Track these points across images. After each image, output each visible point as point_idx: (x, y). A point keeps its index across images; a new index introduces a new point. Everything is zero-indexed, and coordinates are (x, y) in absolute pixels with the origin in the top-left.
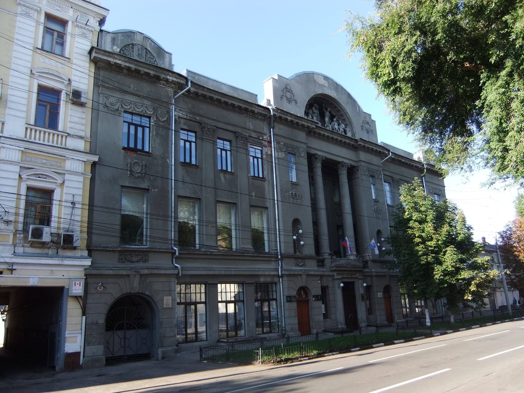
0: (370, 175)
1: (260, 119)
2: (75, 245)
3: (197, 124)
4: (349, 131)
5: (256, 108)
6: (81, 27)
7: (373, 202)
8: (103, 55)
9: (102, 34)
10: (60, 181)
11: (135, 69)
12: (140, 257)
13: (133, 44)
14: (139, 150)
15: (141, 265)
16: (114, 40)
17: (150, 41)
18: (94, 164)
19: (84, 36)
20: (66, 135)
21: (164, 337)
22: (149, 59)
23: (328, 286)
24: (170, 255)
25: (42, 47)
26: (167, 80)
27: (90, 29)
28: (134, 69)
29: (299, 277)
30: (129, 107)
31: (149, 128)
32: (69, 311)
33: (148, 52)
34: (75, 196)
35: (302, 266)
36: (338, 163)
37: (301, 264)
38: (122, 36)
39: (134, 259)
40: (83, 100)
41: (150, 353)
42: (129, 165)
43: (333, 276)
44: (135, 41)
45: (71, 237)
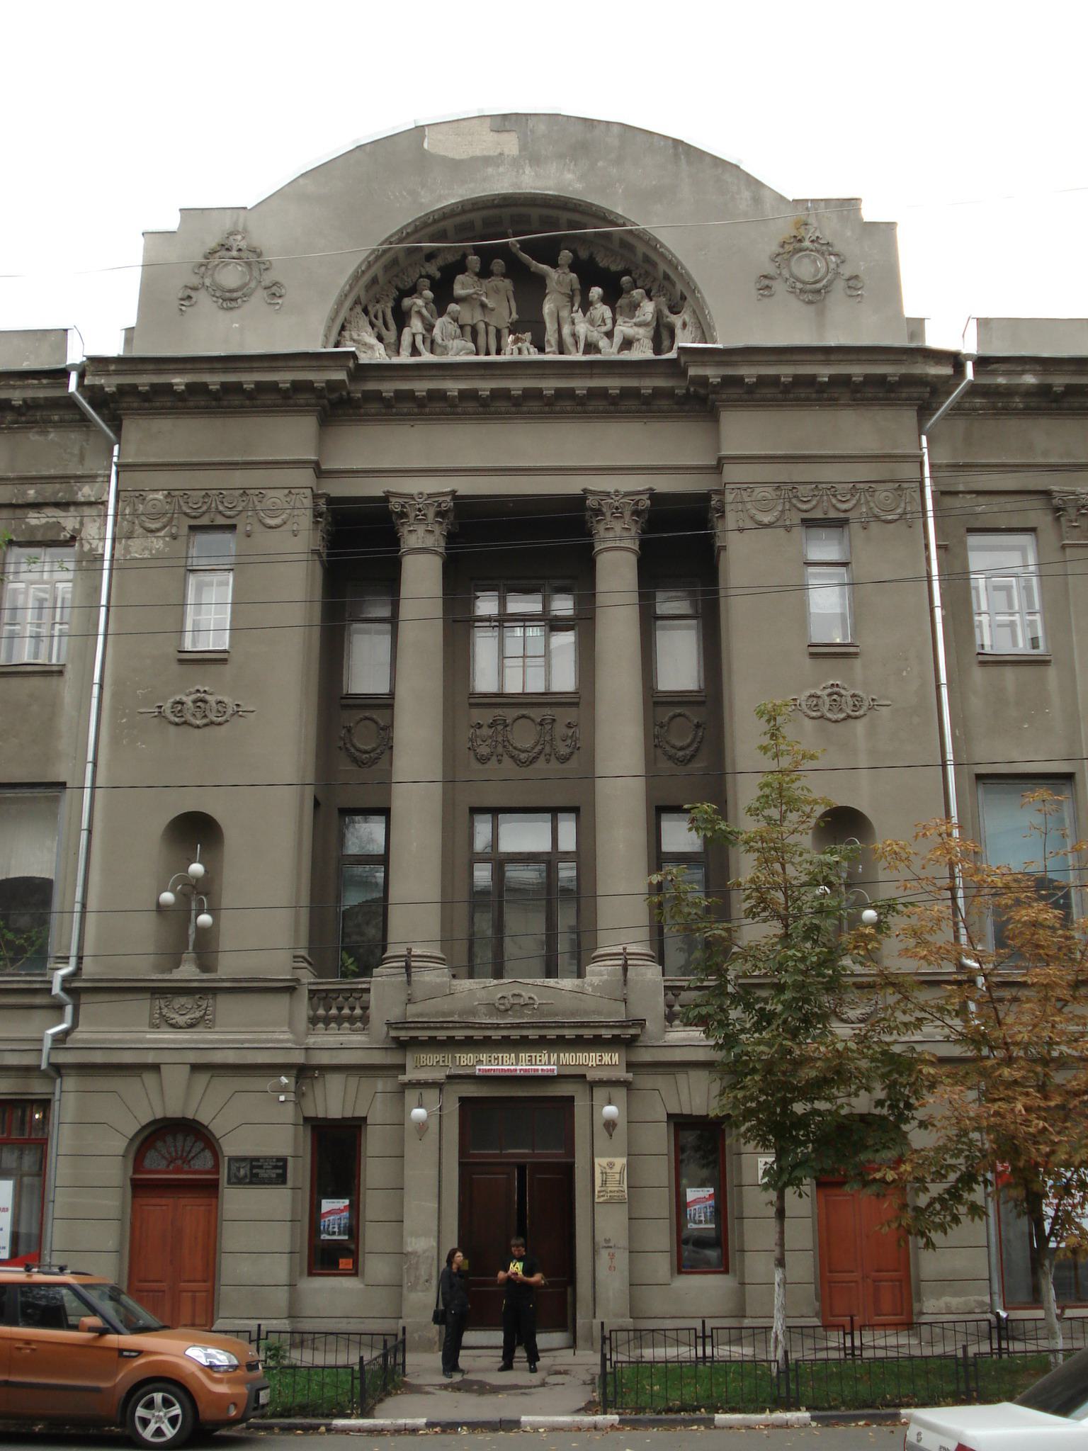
0: (803, 520)
1: (61, 421)
3: (1037, 503)
4: (684, 325)
5: (14, 387)
7: (808, 661)
11: (187, 385)
23: (365, 1119)
28: (183, 387)
35: (191, 1026)
36: (577, 502)
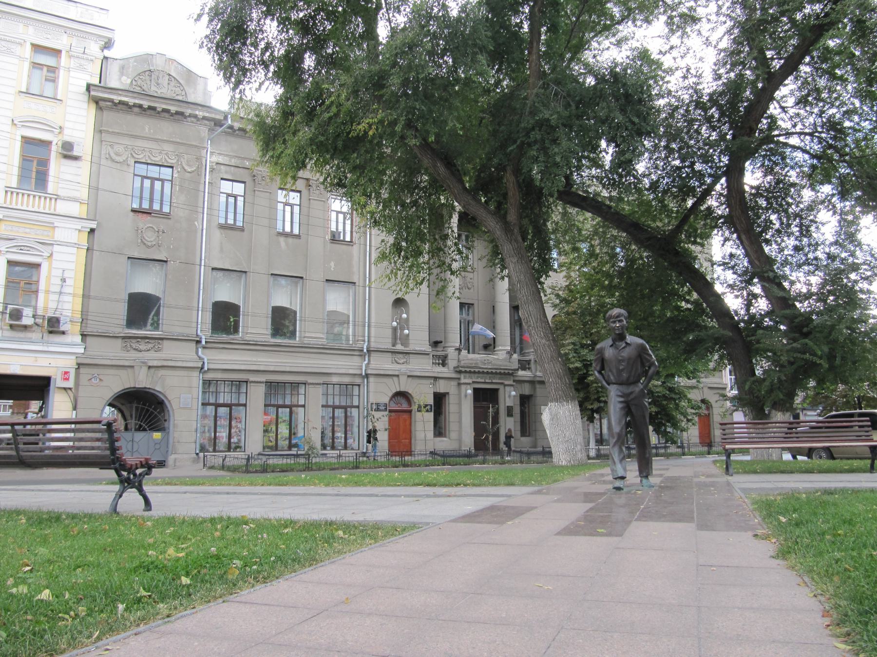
2: (62, 329)
6: (78, 57)
8: (102, 92)
9: (107, 62)
10: (46, 254)
12: (150, 346)
13: (150, 71)
14: (156, 212)
15: (152, 354)
16: (123, 70)
17: (175, 63)
18: (92, 231)
19: (81, 68)
20: (55, 197)
21: (178, 442)
22: (174, 89)
24: (194, 345)
25: (27, 89)
26: (196, 116)
27: (90, 58)
29: (395, 379)
30: (140, 157)
31: (172, 181)
32: (55, 404)
33: (173, 79)
34: (65, 272)
37: (401, 361)
38: (135, 62)
39: (142, 347)
40: (75, 153)
41: (165, 461)
42: (140, 231)
43: (459, 379)
44: (153, 66)
45: (58, 320)
